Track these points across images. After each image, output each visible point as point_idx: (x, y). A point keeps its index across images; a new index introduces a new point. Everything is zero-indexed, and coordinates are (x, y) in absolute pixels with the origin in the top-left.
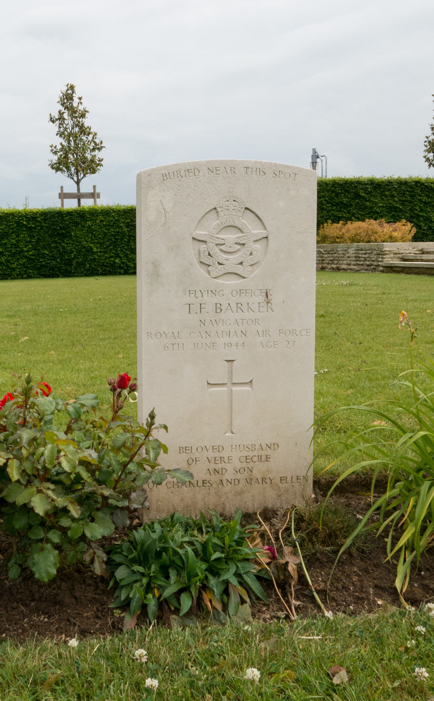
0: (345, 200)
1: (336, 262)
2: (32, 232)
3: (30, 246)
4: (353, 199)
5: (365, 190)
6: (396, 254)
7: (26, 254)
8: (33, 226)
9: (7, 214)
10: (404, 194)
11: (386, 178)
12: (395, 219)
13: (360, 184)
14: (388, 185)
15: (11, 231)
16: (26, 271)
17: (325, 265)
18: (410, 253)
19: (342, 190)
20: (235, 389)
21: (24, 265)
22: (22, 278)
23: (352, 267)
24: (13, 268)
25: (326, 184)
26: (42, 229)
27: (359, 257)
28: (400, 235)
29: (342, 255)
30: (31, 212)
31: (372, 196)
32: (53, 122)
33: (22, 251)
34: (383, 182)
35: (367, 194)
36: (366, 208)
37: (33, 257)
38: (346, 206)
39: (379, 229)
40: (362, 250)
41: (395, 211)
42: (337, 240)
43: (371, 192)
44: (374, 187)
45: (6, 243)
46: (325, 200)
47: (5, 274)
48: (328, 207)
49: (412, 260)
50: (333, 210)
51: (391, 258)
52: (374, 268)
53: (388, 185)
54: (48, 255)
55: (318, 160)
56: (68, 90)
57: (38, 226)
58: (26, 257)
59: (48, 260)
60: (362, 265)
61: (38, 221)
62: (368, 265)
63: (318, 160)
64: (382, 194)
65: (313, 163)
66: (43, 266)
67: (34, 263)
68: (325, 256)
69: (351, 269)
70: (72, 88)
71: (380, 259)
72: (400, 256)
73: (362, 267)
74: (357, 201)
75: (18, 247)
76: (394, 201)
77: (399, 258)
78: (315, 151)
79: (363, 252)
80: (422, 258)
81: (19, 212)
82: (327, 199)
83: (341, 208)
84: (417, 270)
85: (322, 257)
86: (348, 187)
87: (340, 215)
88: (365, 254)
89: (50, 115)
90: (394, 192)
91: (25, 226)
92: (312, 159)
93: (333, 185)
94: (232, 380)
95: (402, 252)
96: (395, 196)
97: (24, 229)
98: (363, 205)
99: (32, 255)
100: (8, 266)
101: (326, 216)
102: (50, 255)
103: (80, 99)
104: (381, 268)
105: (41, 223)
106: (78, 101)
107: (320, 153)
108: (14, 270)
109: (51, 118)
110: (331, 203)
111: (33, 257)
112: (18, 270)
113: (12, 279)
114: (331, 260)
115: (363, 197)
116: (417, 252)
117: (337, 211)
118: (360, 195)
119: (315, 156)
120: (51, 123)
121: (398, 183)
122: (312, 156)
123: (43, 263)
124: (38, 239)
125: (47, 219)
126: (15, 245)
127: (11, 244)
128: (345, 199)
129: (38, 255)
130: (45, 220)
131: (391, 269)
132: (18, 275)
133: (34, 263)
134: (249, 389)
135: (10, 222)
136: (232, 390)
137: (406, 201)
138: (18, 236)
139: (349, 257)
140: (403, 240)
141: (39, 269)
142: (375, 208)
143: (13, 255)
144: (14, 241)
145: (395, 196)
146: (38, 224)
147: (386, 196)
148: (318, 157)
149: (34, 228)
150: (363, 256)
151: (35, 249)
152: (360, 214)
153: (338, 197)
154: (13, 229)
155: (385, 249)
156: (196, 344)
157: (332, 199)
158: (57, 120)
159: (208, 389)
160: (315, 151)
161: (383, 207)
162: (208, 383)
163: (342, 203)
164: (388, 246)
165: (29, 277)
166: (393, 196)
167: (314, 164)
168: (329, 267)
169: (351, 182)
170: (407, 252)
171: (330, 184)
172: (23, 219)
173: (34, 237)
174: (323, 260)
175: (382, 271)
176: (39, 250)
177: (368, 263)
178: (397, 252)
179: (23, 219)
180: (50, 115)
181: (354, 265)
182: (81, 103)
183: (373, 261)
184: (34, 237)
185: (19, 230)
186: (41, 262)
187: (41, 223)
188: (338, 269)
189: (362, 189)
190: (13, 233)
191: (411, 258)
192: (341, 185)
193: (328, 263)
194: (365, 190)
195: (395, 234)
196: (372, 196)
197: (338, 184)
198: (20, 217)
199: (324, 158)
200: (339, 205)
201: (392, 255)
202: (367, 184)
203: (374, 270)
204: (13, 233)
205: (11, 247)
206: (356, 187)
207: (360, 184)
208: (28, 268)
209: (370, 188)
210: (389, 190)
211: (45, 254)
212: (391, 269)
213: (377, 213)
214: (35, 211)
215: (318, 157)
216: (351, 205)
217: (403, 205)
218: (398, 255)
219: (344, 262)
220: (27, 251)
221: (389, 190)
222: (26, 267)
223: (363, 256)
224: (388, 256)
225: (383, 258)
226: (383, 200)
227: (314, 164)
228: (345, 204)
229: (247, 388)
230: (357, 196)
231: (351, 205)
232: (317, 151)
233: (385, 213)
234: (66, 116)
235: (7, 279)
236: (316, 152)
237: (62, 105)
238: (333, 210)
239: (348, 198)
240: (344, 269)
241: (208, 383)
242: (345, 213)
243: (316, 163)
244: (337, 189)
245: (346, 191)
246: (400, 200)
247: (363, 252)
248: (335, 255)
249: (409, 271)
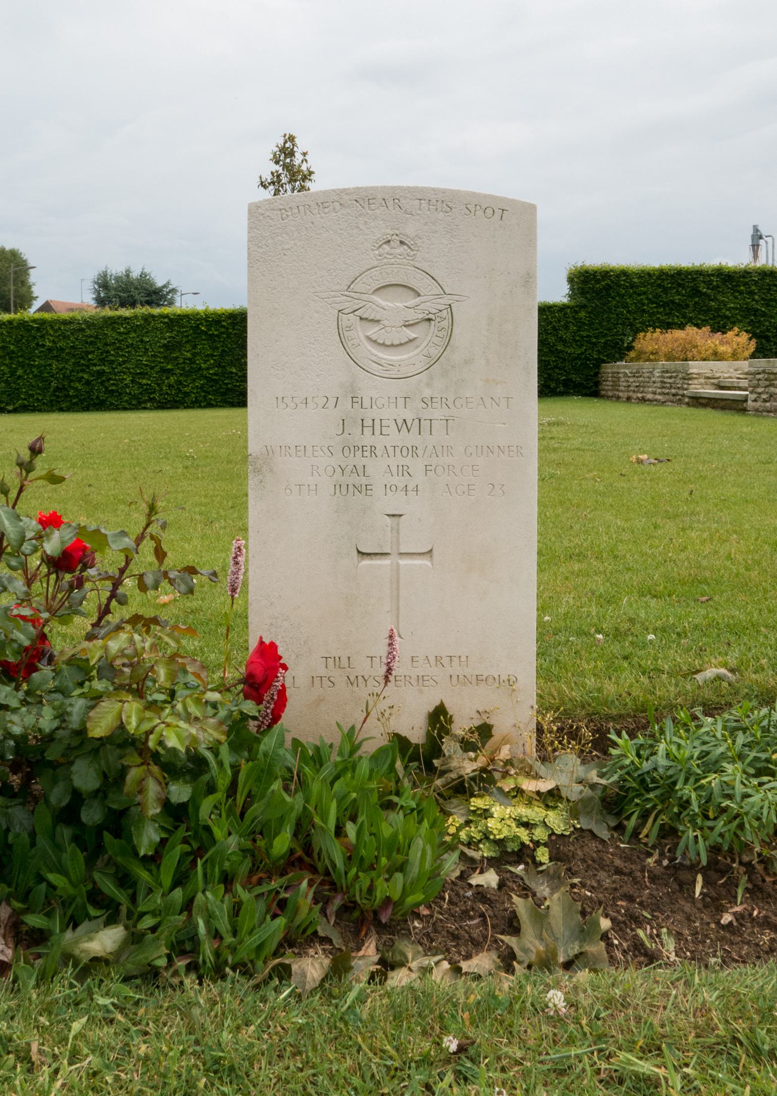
0: (677, 298)
1: (642, 389)
2: (215, 341)
3: (212, 362)
4: (690, 296)
5: (709, 284)
6: (709, 378)
7: (205, 372)
8: (216, 333)
9: (179, 315)
10: (769, 290)
11: (743, 267)
12: (720, 327)
13: (701, 274)
14: (744, 277)
15: (184, 340)
16: (205, 396)
17: (631, 394)
18: (731, 378)
19: (672, 283)
20: (404, 562)
21: (202, 388)
22: (200, 407)
23: (658, 397)
24: (185, 393)
25: (649, 274)
26: (228, 337)
27: (665, 383)
28: (730, 350)
29: (647, 380)
30: (215, 313)
31: (719, 292)
32: (265, 187)
33: (200, 369)
34: (735, 272)
35: (712, 289)
36: (710, 309)
37: (215, 377)
38: (680, 306)
39: (699, 341)
40: (667, 372)
41: (755, 315)
42: (652, 357)
43: (718, 287)
44: (722, 279)
45: (177, 357)
46: (647, 299)
47: (176, 401)
48: (651, 308)
49: (729, 388)
50: (658, 313)
51: (701, 384)
52: (680, 400)
53: (744, 277)
54: (236, 374)
55: (762, 242)
56: (285, 142)
57: (223, 333)
58: (206, 377)
59: (237, 381)
60: (668, 394)
61: (223, 326)
62: (674, 395)
63: (762, 242)
64: (734, 289)
65: (753, 246)
66: (231, 390)
67: (218, 386)
68: (631, 380)
69: (656, 400)
70: (292, 139)
71: (686, 386)
72: (715, 381)
73: (667, 397)
74: (697, 299)
75: (194, 363)
76: (754, 300)
77: (713, 384)
78: (756, 229)
79: (668, 375)
80: (741, 385)
81: (198, 314)
82: (650, 296)
83: (672, 309)
84: (722, 403)
85: (628, 381)
86: (683, 280)
87: (670, 320)
88: (671, 377)
89: (260, 178)
90: (753, 288)
91: (205, 333)
92: (753, 240)
93: (660, 276)
94: (398, 549)
95: (717, 375)
96: (755, 294)
97: (204, 337)
98: (706, 306)
99: (214, 374)
100: (178, 388)
101: (649, 321)
102: (239, 374)
103: (304, 154)
104: (687, 400)
105: (227, 329)
106: (302, 157)
107: (764, 231)
108: (187, 394)
109: (262, 183)
110: (656, 303)
111: (215, 377)
112: (193, 395)
113: (185, 408)
114: (637, 387)
115: (705, 293)
116: (741, 376)
117: (666, 314)
118: (700, 292)
119: (757, 237)
120: (261, 188)
121: (760, 274)
122: (753, 236)
123: (229, 386)
124: (223, 351)
125: (237, 324)
126: (189, 359)
127: (185, 359)
128: (677, 297)
129: (223, 374)
130: (233, 324)
131: (698, 402)
132: (193, 402)
133: (218, 386)
134: (428, 563)
135: (184, 327)
136: (398, 564)
137: (771, 300)
138: (195, 347)
139: (654, 382)
140: (735, 356)
141: (224, 394)
142: (724, 311)
143: (187, 374)
144: (189, 355)
145: (755, 294)
146: (223, 330)
147: (741, 293)
148: (761, 237)
149: (217, 336)
150: (669, 380)
151: (219, 366)
152: (700, 319)
153: (667, 294)
154: (187, 336)
155: (691, 371)
156: (338, 487)
157: (657, 296)
158: (270, 184)
159: (359, 562)
160: (756, 229)
161: (736, 309)
162: (359, 552)
163: (673, 302)
164: (695, 367)
165: (209, 405)
166: (752, 293)
167: (755, 247)
168: (635, 396)
169: (686, 272)
170: (726, 375)
171: (654, 274)
172: (201, 324)
173: (217, 348)
174: (629, 386)
175: (688, 404)
176: (224, 367)
177: (673, 391)
178: (710, 375)
179: (201, 324)
180: (260, 178)
181: (660, 394)
182: (306, 161)
183: (678, 388)
184: (217, 348)
185: (196, 338)
186: (226, 384)
187: (227, 329)
188: (643, 400)
189: (704, 282)
190: (187, 342)
191: (727, 385)
192: (672, 276)
193: (634, 391)
194: (709, 284)
195: (722, 349)
196: (719, 292)
197: (667, 274)
198: (198, 320)
199: (769, 240)
200: (668, 305)
201: (702, 381)
202: (713, 275)
203: (680, 402)
204: (187, 342)
205: (184, 363)
206: (694, 279)
207: (701, 274)
208: (209, 393)
209: (715, 281)
210: (745, 284)
211: (232, 373)
212: (698, 402)
213: (728, 318)
214: (219, 312)
215: (761, 237)
216: (688, 306)
217: (768, 305)
218: (712, 381)
219: (650, 389)
220: (208, 369)
221: (745, 284)
222: (204, 391)
223: (669, 380)
224: (696, 382)
225: (689, 384)
226: (736, 298)
227: (755, 247)
228: (679, 305)
229: (425, 562)
230: (696, 292)
231: (688, 306)
232: (759, 228)
233: (739, 317)
234: (284, 180)
235: (177, 408)
236: (757, 231)
237: (277, 163)
238: (658, 313)
239: (683, 296)
240: (649, 400)
241: (359, 552)
242: (678, 317)
243: (758, 245)
244: (666, 282)
245: (679, 285)
246: (763, 299)
247: (668, 375)
248: (641, 379)
249: (716, 405)
